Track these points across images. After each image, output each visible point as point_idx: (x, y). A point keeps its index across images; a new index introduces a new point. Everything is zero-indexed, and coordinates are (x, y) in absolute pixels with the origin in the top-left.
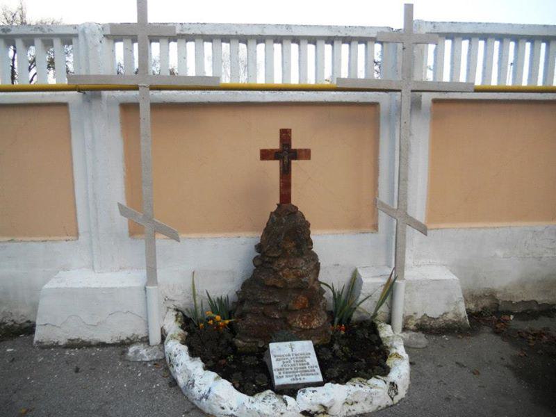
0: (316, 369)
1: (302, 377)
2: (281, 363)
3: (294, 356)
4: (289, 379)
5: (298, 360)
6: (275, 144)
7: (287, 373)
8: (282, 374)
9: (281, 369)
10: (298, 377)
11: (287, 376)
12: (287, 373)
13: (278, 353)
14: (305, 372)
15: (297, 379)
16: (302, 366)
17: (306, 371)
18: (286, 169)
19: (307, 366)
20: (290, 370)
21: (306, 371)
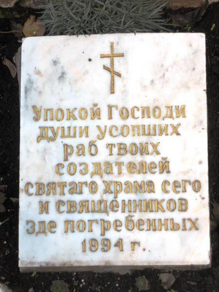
0: (190, 195)
1: (127, 236)
2: (56, 150)
3: (117, 121)
4: (78, 238)
5: (128, 140)
6: (107, 51)
7: (72, 207)
8: (52, 215)
9: (52, 186)
10: (113, 235)
11: (70, 227)
12: (72, 207)
13: (49, 101)
14: (146, 212)
15: (106, 245)
16: (139, 178)
17: (148, 206)
18: (103, 233)
19: (158, 179)
20: (86, 195)
21: (148, 206)
